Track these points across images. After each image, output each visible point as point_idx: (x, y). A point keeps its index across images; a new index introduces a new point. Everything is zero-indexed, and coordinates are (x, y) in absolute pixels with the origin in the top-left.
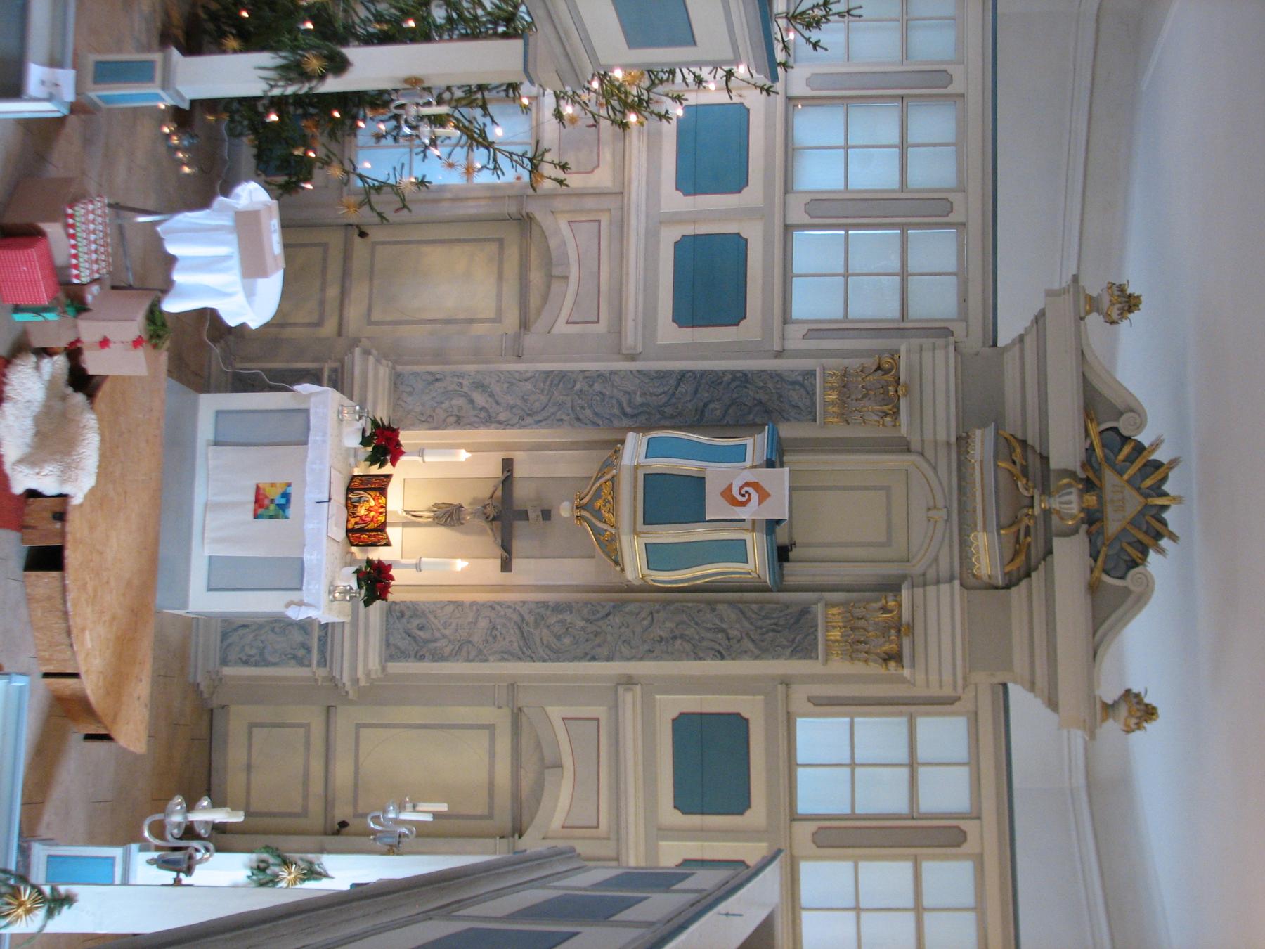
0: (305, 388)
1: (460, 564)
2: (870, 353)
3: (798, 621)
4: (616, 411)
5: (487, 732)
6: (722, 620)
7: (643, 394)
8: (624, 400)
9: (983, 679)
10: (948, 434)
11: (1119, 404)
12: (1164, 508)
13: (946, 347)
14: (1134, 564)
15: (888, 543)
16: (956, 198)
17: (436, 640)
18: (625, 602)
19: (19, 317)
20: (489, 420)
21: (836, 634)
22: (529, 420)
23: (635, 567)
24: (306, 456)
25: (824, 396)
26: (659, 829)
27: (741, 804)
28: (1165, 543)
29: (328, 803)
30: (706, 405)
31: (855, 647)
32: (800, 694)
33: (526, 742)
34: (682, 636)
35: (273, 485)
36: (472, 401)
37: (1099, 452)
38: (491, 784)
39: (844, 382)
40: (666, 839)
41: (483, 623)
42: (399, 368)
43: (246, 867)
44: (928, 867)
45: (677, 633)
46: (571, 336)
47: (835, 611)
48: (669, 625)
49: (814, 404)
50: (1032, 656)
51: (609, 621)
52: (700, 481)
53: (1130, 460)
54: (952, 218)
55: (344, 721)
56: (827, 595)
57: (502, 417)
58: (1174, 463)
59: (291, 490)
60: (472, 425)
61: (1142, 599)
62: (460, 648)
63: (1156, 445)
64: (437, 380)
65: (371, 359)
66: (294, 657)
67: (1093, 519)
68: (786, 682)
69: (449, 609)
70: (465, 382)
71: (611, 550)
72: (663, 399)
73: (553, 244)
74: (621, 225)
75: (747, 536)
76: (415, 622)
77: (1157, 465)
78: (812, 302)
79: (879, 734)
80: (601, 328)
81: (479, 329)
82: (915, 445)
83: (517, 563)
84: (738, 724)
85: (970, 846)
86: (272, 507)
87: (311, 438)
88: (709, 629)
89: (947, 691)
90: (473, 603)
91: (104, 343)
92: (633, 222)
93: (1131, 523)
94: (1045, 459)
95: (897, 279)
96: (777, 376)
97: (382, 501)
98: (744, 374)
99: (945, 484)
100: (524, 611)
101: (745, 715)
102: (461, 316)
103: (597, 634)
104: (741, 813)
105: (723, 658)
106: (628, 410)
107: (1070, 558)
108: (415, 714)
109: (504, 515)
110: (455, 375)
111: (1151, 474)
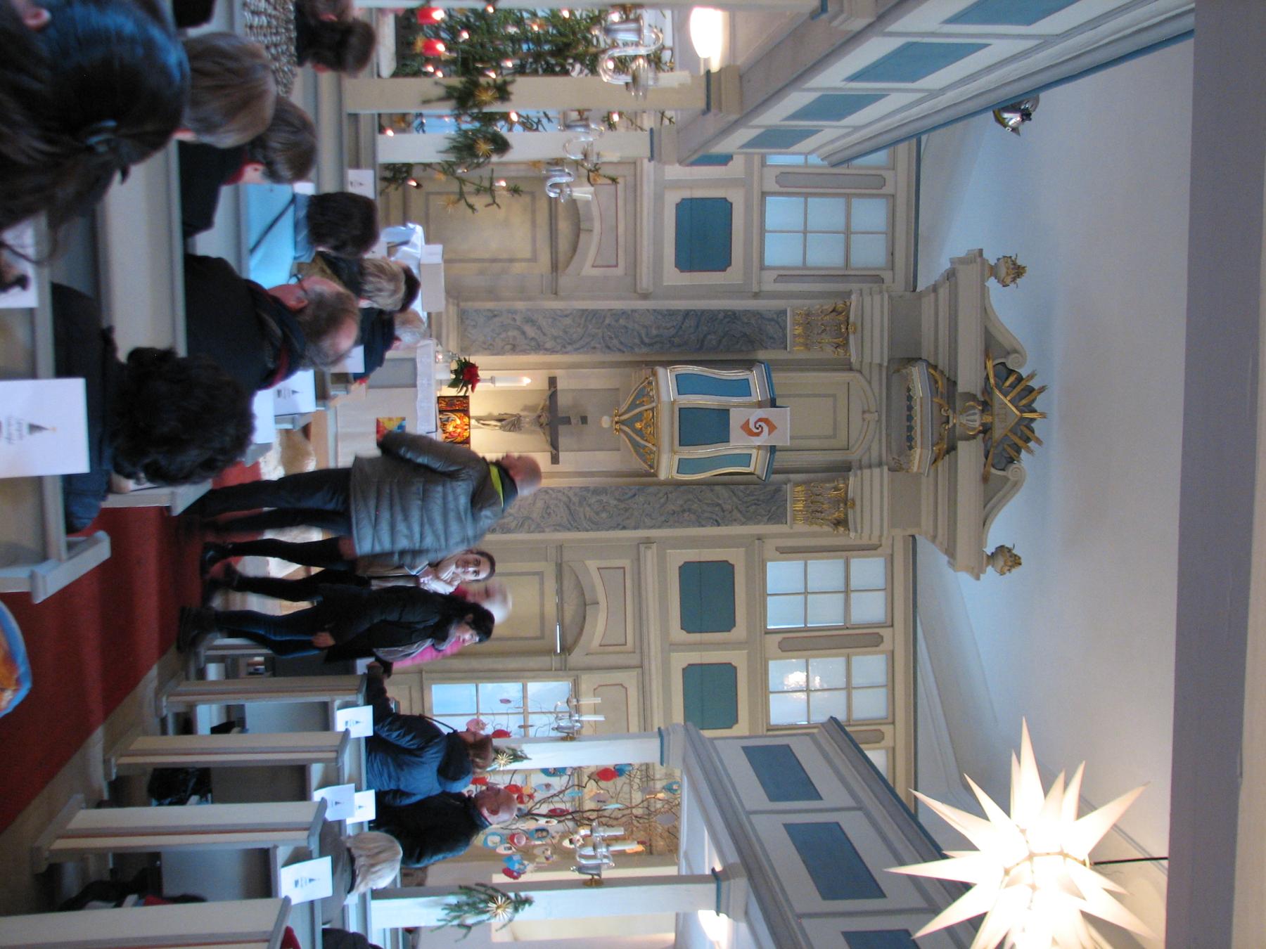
4: (637, 341)
5: (537, 577)
6: (718, 497)
9: (899, 533)
10: (882, 359)
11: (1007, 345)
12: (1032, 420)
13: (881, 292)
14: (1011, 461)
15: (834, 436)
16: (888, 175)
20: (538, 348)
21: (800, 506)
22: (569, 348)
23: (667, 469)
24: (416, 397)
25: (793, 329)
27: (729, 624)
28: (1032, 444)
30: (705, 336)
31: (813, 513)
32: (770, 545)
33: (568, 584)
34: (689, 510)
35: (390, 419)
36: (524, 333)
37: (992, 381)
38: (542, 617)
39: (808, 321)
40: (675, 651)
41: (540, 504)
44: (856, 660)
45: (685, 507)
46: (594, 281)
47: (799, 488)
48: (680, 502)
49: (785, 336)
51: (634, 498)
52: (724, 414)
53: (1013, 386)
56: (792, 476)
57: (548, 345)
58: (1042, 389)
60: (524, 352)
61: (1016, 485)
63: (1031, 377)
64: (495, 316)
68: (760, 538)
70: (518, 318)
71: (649, 457)
72: (673, 331)
75: (754, 452)
77: (1031, 390)
79: (825, 571)
80: (619, 271)
81: (518, 268)
82: (856, 365)
83: (562, 455)
84: (726, 569)
88: (708, 505)
89: (875, 541)
92: (645, 188)
93: (1011, 431)
94: (953, 383)
96: (757, 314)
98: (734, 313)
99: (877, 391)
100: (571, 494)
102: (505, 256)
103: (626, 510)
105: (719, 525)
106: (647, 340)
107: (969, 455)
109: (553, 418)
110: (509, 311)
111: (1026, 393)
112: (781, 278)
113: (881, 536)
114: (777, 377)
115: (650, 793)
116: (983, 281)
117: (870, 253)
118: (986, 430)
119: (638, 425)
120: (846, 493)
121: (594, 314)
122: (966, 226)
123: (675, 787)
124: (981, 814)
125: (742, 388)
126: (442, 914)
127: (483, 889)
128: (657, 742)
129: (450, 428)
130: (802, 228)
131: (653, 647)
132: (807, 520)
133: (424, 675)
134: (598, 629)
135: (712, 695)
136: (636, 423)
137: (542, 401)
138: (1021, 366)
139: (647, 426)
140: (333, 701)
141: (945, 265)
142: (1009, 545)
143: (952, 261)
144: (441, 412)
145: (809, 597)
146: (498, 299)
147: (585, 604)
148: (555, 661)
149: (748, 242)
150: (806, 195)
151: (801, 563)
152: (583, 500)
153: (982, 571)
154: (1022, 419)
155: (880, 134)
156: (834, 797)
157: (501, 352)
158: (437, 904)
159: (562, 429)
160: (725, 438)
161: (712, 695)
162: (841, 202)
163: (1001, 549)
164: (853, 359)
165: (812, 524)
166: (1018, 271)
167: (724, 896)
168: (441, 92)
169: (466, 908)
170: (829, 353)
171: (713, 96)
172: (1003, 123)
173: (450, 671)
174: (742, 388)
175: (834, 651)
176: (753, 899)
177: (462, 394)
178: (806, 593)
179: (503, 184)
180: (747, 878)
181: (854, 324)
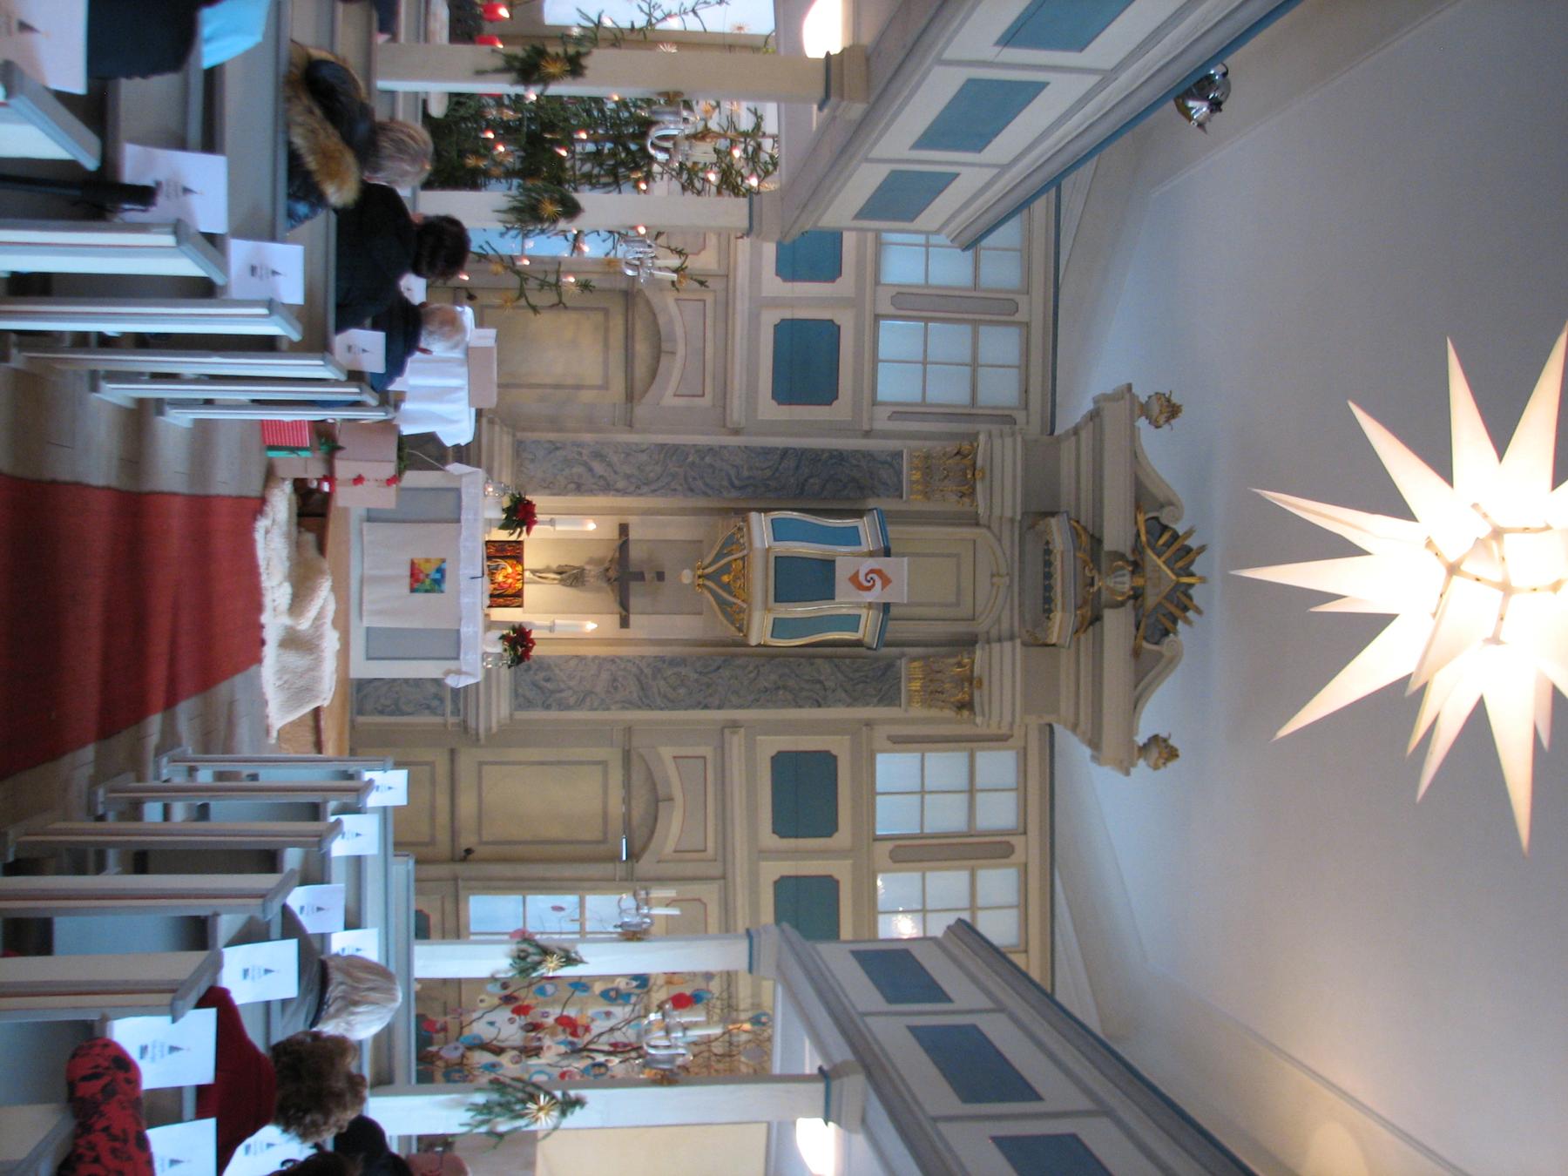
0: (455, 468)
1: (590, 626)
2: (951, 436)
3: (883, 674)
4: (725, 483)
7: (750, 468)
8: (733, 473)
9: (1034, 722)
12: (1191, 585)
13: (1013, 434)
14: (1166, 633)
15: (958, 604)
17: (561, 691)
18: (734, 656)
19: (272, 454)
20: (607, 488)
21: (916, 685)
22: (645, 489)
23: (760, 630)
25: (910, 475)
26: (761, 852)
27: (830, 828)
28: (1191, 614)
29: (454, 833)
31: (932, 695)
32: (881, 732)
33: (638, 778)
34: (785, 688)
35: (428, 561)
36: (591, 470)
37: (1143, 538)
39: (927, 465)
41: (605, 676)
42: (519, 435)
43: (508, 956)
46: (676, 410)
47: (916, 664)
48: (773, 677)
49: (901, 482)
50: (1077, 704)
51: (722, 672)
52: (828, 565)
53: (1168, 545)
54: (1018, 317)
55: (467, 760)
56: (906, 650)
57: (621, 484)
58: (1202, 549)
59: (446, 566)
60: (591, 492)
61: (1173, 661)
62: (583, 700)
63: (1189, 534)
65: (497, 428)
66: (428, 707)
67: (1137, 595)
68: (869, 724)
69: (573, 663)
70: (585, 452)
71: (736, 616)
72: (768, 473)
73: (662, 320)
74: (726, 306)
75: (863, 612)
76: (542, 675)
77: (1188, 550)
78: (895, 385)
79: (945, 766)
80: (707, 401)
81: (587, 396)
83: (633, 618)
84: (827, 761)
85: (1018, 857)
86: (428, 582)
87: (463, 517)
89: (1004, 730)
90: (595, 658)
91: (359, 480)
92: (739, 306)
93: (1165, 598)
94: (1097, 541)
95: (968, 369)
96: (868, 456)
97: (519, 568)
101: (834, 752)
102: (570, 382)
103: (708, 686)
104: (830, 835)
106: (737, 482)
107: (1117, 625)
108: (534, 754)
109: (621, 575)
110: (575, 444)
111: (1183, 555)
112: (896, 416)
113: (1012, 725)
114: (893, 531)
115: (734, 1022)
116: (1132, 421)
117: (1000, 390)
118: (1137, 595)
119: (725, 579)
120: (972, 671)
121: (674, 451)
122: (1107, 364)
123: (764, 1019)
124: (1342, 548)
125: (852, 537)
126: (467, 1116)
127: (520, 1085)
128: (745, 944)
129: (500, 578)
130: (920, 358)
131: (738, 854)
132: (924, 702)
133: (461, 883)
134: (673, 830)
135: (809, 908)
136: (723, 579)
137: (609, 553)
138: (1177, 520)
139: (736, 578)
140: (326, 802)
141: (1087, 406)
142: (1163, 734)
143: (1096, 401)
144: (489, 558)
145: (927, 797)
146: (560, 430)
147: (658, 799)
148: (620, 870)
149: (858, 354)
150: (927, 320)
151: (918, 755)
152: (657, 671)
153: (1133, 765)
154: (1178, 584)
155: (1029, 175)
156: (965, 997)
157: (563, 492)
158: (459, 1104)
159: (634, 586)
160: (828, 594)
161: (809, 908)
162: (966, 330)
163: (1155, 739)
164: (981, 511)
165: (930, 706)
166: (1173, 411)
167: (834, 1097)
168: (499, 62)
169: (497, 1109)
170: (951, 504)
171: (834, 85)
172: (1186, 113)
173: (490, 879)
174: (852, 537)
175: (957, 863)
176: (871, 1091)
177: (514, 538)
178: (923, 792)
179: (572, 280)
180: (857, 1078)
181: (983, 469)
